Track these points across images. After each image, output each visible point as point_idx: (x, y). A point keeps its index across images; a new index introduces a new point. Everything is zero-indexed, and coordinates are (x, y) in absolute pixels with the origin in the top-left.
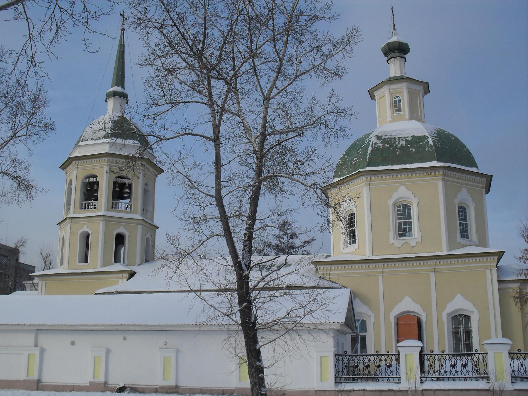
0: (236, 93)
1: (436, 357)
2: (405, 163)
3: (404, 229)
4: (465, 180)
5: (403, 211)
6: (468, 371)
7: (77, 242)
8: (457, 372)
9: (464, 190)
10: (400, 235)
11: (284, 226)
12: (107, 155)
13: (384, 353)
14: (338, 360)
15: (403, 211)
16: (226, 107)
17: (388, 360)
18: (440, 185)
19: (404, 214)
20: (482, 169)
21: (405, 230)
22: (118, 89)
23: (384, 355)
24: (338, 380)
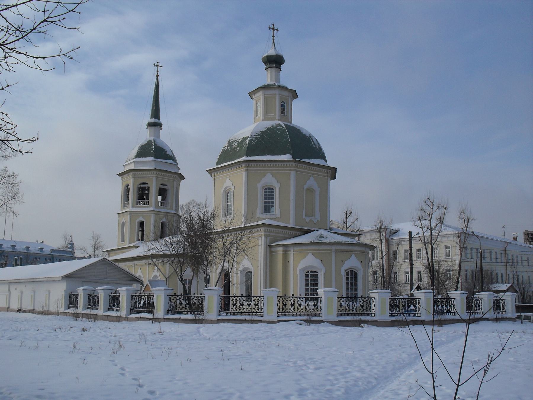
0: (442, 224)
1: (238, 299)
3: (268, 207)
4: (318, 171)
5: (269, 192)
6: (236, 309)
7: (136, 227)
8: (258, 309)
12: (155, 170)
15: (269, 192)
16: (419, 222)
17: (285, 301)
18: (293, 174)
19: (269, 195)
20: (330, 163)
21: (269, 207)
22: (156, 121)
23: (297, 297)
24: (165, 314)
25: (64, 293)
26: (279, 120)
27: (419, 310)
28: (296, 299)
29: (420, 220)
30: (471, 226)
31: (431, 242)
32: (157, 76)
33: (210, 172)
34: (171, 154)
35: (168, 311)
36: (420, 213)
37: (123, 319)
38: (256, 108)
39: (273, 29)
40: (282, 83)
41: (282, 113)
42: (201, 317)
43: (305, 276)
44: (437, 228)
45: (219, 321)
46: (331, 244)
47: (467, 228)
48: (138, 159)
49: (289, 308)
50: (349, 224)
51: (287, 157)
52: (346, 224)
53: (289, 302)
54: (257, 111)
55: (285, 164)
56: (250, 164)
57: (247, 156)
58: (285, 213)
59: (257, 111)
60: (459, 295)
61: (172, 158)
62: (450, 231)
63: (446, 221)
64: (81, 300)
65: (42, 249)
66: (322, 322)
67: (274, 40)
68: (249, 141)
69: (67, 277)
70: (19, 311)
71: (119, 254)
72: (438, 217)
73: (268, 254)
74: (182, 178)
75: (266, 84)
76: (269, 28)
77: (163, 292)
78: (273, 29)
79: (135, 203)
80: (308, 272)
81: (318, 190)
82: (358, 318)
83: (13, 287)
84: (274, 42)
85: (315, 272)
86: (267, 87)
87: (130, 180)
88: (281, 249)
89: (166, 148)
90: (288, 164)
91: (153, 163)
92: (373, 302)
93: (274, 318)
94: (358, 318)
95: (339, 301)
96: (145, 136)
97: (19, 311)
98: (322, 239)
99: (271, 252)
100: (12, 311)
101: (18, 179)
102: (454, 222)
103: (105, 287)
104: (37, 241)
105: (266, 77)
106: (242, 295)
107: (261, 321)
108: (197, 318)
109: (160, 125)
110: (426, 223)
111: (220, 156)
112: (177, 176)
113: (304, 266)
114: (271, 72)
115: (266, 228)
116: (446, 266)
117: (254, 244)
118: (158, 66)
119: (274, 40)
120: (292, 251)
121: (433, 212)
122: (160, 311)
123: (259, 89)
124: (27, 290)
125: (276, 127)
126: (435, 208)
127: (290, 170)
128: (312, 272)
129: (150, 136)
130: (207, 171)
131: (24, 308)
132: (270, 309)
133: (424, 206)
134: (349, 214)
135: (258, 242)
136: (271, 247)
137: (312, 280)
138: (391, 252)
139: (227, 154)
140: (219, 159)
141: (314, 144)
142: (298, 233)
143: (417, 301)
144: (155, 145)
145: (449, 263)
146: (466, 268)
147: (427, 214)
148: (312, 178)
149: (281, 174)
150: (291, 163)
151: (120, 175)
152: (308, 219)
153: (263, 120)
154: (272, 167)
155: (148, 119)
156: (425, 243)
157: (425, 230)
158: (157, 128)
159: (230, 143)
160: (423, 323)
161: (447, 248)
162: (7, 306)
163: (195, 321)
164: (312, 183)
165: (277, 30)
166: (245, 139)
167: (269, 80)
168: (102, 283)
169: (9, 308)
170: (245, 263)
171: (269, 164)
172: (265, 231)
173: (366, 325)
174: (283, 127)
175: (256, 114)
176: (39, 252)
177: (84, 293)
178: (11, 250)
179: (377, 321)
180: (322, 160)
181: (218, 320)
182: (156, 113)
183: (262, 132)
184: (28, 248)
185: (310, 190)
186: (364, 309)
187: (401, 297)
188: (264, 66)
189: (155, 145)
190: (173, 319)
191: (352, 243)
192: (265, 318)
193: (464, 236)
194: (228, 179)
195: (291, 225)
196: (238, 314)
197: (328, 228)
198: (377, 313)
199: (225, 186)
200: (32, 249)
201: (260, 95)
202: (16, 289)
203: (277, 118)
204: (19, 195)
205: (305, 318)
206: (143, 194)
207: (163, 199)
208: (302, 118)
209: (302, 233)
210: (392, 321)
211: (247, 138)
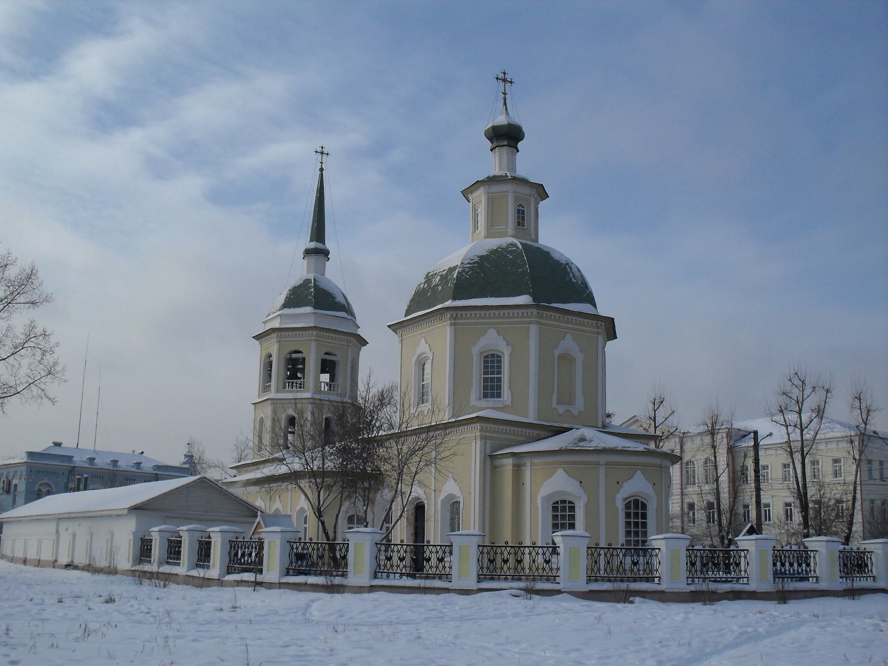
1: (602, 552)
2: (484, 295)
3: (492, 389)
5: (492, 362)
9: (569, 337)
10: (485, 396)
11: (812, 411)
12: (315, 328)
13: (528, 543)
14: (482, 553)
15: (492, 362)
17: (492, 553)
18: (534, 330)
19: (493, 367)
20: (603, 310)
22: (320, 245)
23: (603, 548)
24: (282, 576)
25: (131, 537)
26: (513, 236)
27: (745, 571)
28: (499, 551)
29: (782, 411)
30: (873, 422)
31: (802, 450)
32: (322, 170)
33: (395, 327)
34: (343, 301)
35: (288, 569)
36: (783, 400)
37: (215, 582)
38: (475, 216)
39: (505, 80)
40: (521, 171)
41: (519, 224)
42: (337, 580)
43: (551, 509)
44: (813, 425)
45: (372, 589)
46: (597, 451)
47: (866, 424)
48: (287, 311)
49: (498, 566)
50: (659, 420)
51: (523, 299)
52: (655, 421)
53: (499, 556)
54: (476, 222)
55: (520, 311)
56: (459, 313)
57: (454, 299)
58: (521, 400)
59: (476, 222)
60: (824, 543)
61: (346, 308)
62: (839, 432)
63: (830, 411)
64: (157, 550)
65: (138, 464)
66: (559, 592)
67: (505, 99)
68: (459, 272)
69: (136, 509)
70: (68, 566)
71: (247, 471)
72: (814, 406)
73: (488, 471)
74: (364, 342)
75: (491, 175)
76: (497, 78)
77: (279, 535)
78: (505, 80)
79: (281, 386)
80: (557, 503)
81: (579, 357)
82: (623, 586)
83: (63, 526)
84: (505, 103)
85: (570, 502)
86: (492, 180)
87: (273, 346)
88: (509, 462)
89: (331, 291)
90: (525, 311)
91: (312, 317)
92: (657, 555)
93: (472, 584)
94: (623, 586)
95: (592, 555)
96: (299, 271)
97: (68, 566)
98: (582, 444)
99: (494, 468)
100: (60, 567)
101: (53, 340)
102: (842, 414)
103: (163, 527)
104: (134, 451)
105: (492, 163)
106: (402, 541)
107: (447, 590)
108: (329, 583)
109: (325, 253)
110: (792, 417)
111: (412, 300)
112: (353, 339)
113: (550, 492)
114: (500, 155)
115: (484, 425)
116: (833, 493)
117: (452, 451)
118: (322, 153)
119: (505, 99)
120: (529, 464)
121: (805, 397)
122: (272, 570)
123: (478, 184)
124: (82, 530)
125: (507, 247)
126: (808, 391)
127: (530, 323)
128: (564, 502)
129: (308, 271)
130: (389, 326)
131: (76, 562)
132: (464, 567)
133: (788, 387)
134: (658, 403)
135: (469, 448)
136: (492, 457)
137: (563, 517)
138: (738, 468)
139: (420, 299)
140: (409, 307)
141: (574, 276)
142: (543, 433)
143: (812, 555)
144: (316, 286)
145: (839, 488)
146: (872, 497)
147: (794, 402)
148: (569, 337)
149: (515, 333)
150: (530, 311)
151: (257, 337)
152: (561, 409)
153: (485, 238)
154: (496, 318)
155: (306, 243)
156: (791, 453)
157: (790, 429)
158: (321, 257)
159: (428, 278)
160: (753, 596)
161: (836, 461)
162: (54, 559)
163: (331, 589)
164: (568, 344)
165: (511, 82)
166: (451, 270)
167: (497, 168)
168: (187, 519)
169: (56, 561)
170: (450, 488)
171: (492, 312)
172: (481, 430)
173: (637, 599)
174: (518, 248)
175: (476, 227)
176: (134, 470)
177: (161, 537)
178: (87, 465)
179: (663, 592)
180: (589, 305)
181: (372, 586)
182: (318, 231)
183: (482, 258)
184: (115, 462)
185: (566, 359)
186: (696, 571)
187: (700, 547)
188: (489, 145)
189: (316, 286)
190: (294, 584)
191: (652, 451)
192: (455, 584)
193: (865, 438)
194: (423, 340)
195: (531, 419)
196: (434, 578)
197: (600, 425)
198: (664, 578)
199: (418, 352)
200: (123, 465)
201: (480, 196)
202: (67, 529)
203: (510, 231)
204: (59, 368)
205: (522, 584)
206: (294, 368)
207: (332, 379)
208: (559, 234)
209: (550, 434)
210: (691, 592)
211: (455, 268)
